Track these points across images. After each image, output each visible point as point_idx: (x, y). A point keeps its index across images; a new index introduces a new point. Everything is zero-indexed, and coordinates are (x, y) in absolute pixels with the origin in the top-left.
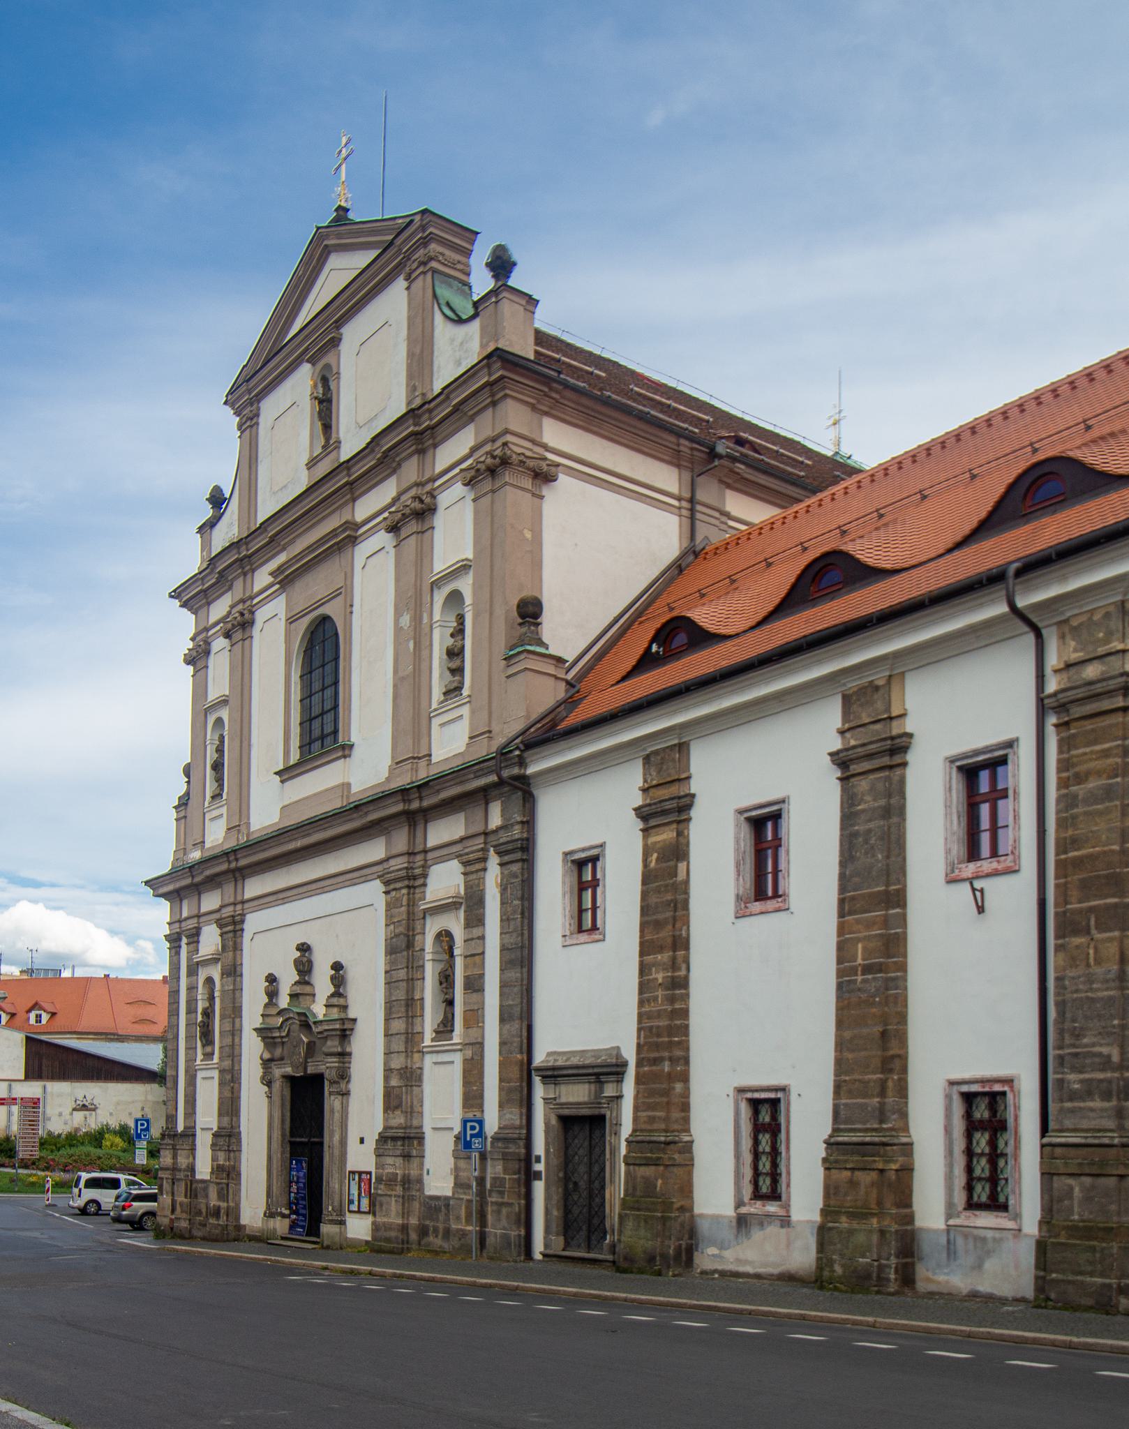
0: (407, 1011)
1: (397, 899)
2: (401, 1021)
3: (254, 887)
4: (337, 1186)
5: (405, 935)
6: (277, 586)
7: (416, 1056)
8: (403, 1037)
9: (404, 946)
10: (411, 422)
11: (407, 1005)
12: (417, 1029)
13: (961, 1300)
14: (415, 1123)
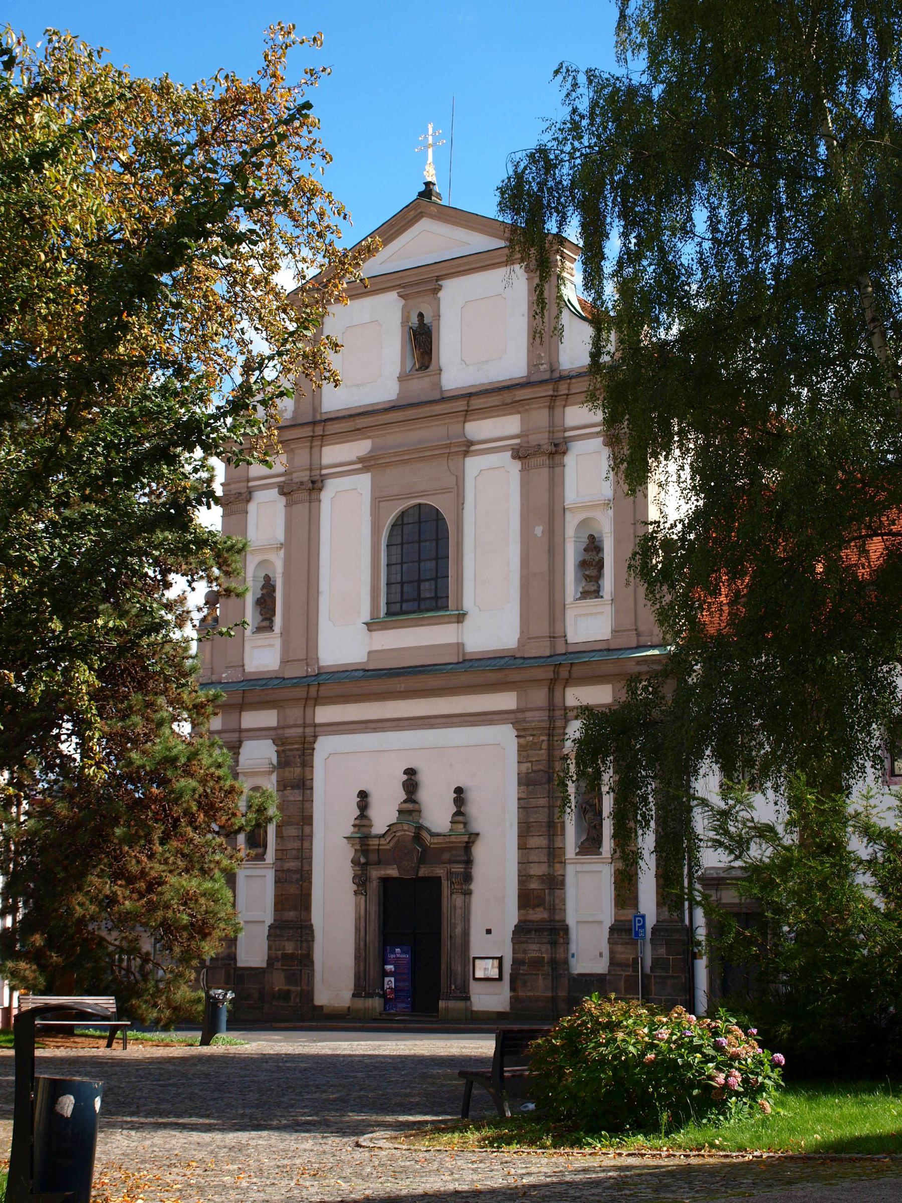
0: (549, 831)
1: (535, 744)
2: (541, 838)
3: (325, 714)
4: (459, 969)
5: (545, 772)
6: (359, 466)
7: (557, 866)
8: (545, 851)
9: (544, 780)
10: (551, 387)
11: (549, 827)
12: (558, 844)
13: (801, 1178)
14: (557, 918)
